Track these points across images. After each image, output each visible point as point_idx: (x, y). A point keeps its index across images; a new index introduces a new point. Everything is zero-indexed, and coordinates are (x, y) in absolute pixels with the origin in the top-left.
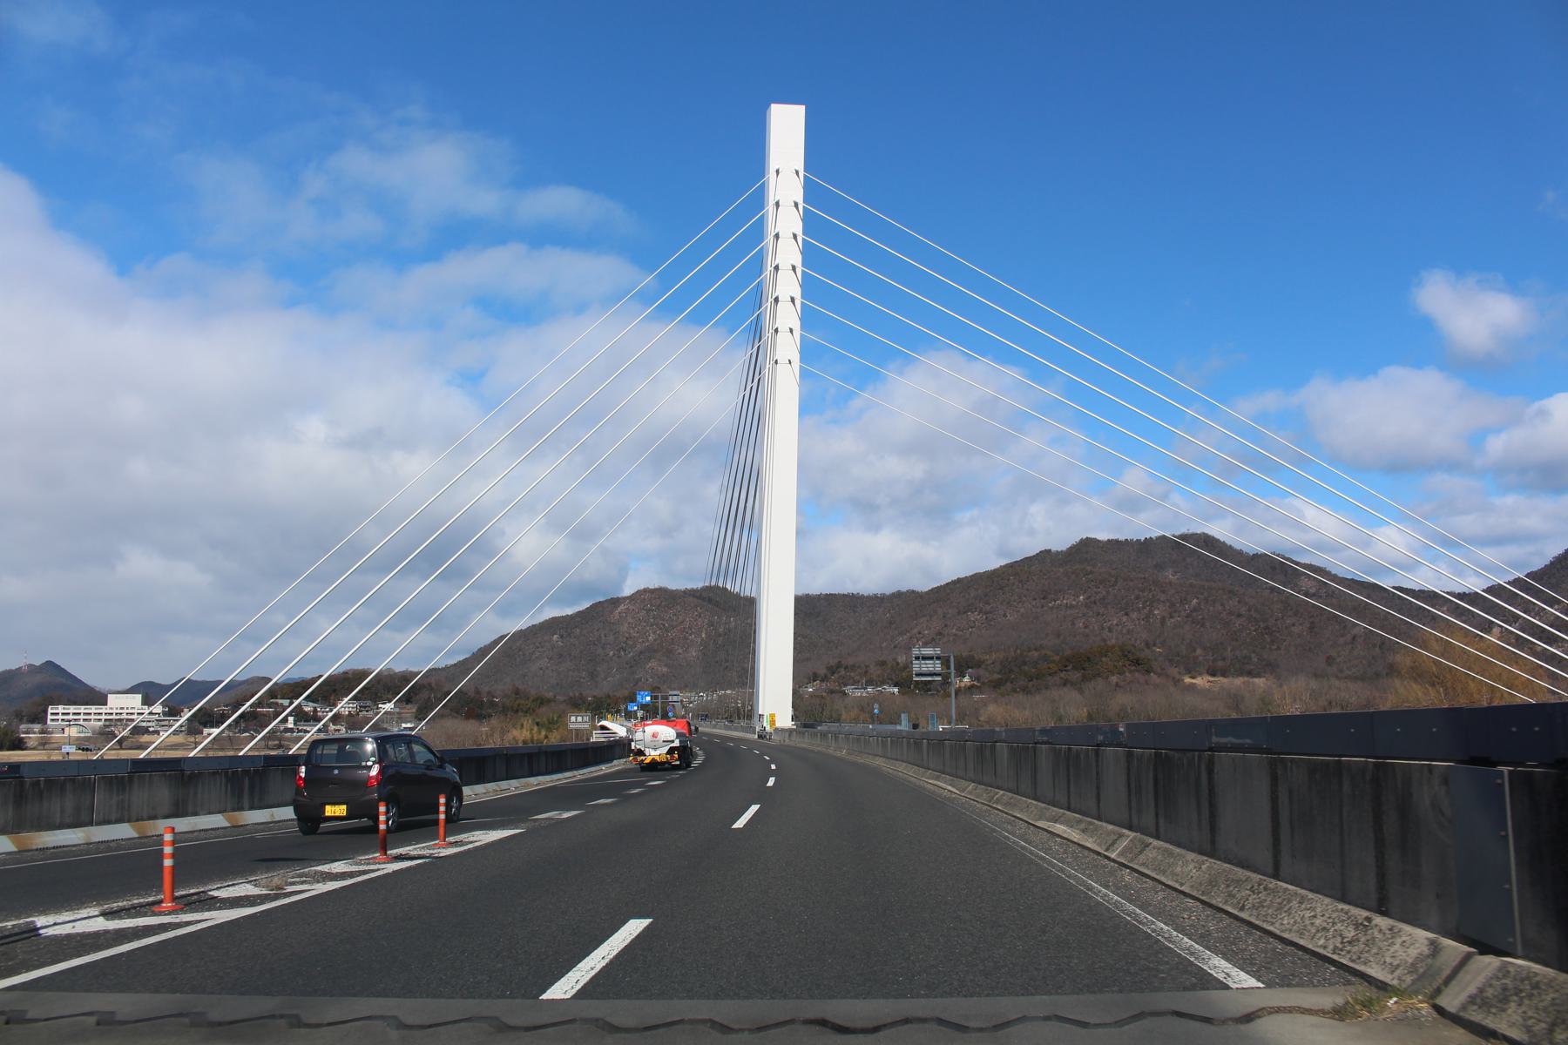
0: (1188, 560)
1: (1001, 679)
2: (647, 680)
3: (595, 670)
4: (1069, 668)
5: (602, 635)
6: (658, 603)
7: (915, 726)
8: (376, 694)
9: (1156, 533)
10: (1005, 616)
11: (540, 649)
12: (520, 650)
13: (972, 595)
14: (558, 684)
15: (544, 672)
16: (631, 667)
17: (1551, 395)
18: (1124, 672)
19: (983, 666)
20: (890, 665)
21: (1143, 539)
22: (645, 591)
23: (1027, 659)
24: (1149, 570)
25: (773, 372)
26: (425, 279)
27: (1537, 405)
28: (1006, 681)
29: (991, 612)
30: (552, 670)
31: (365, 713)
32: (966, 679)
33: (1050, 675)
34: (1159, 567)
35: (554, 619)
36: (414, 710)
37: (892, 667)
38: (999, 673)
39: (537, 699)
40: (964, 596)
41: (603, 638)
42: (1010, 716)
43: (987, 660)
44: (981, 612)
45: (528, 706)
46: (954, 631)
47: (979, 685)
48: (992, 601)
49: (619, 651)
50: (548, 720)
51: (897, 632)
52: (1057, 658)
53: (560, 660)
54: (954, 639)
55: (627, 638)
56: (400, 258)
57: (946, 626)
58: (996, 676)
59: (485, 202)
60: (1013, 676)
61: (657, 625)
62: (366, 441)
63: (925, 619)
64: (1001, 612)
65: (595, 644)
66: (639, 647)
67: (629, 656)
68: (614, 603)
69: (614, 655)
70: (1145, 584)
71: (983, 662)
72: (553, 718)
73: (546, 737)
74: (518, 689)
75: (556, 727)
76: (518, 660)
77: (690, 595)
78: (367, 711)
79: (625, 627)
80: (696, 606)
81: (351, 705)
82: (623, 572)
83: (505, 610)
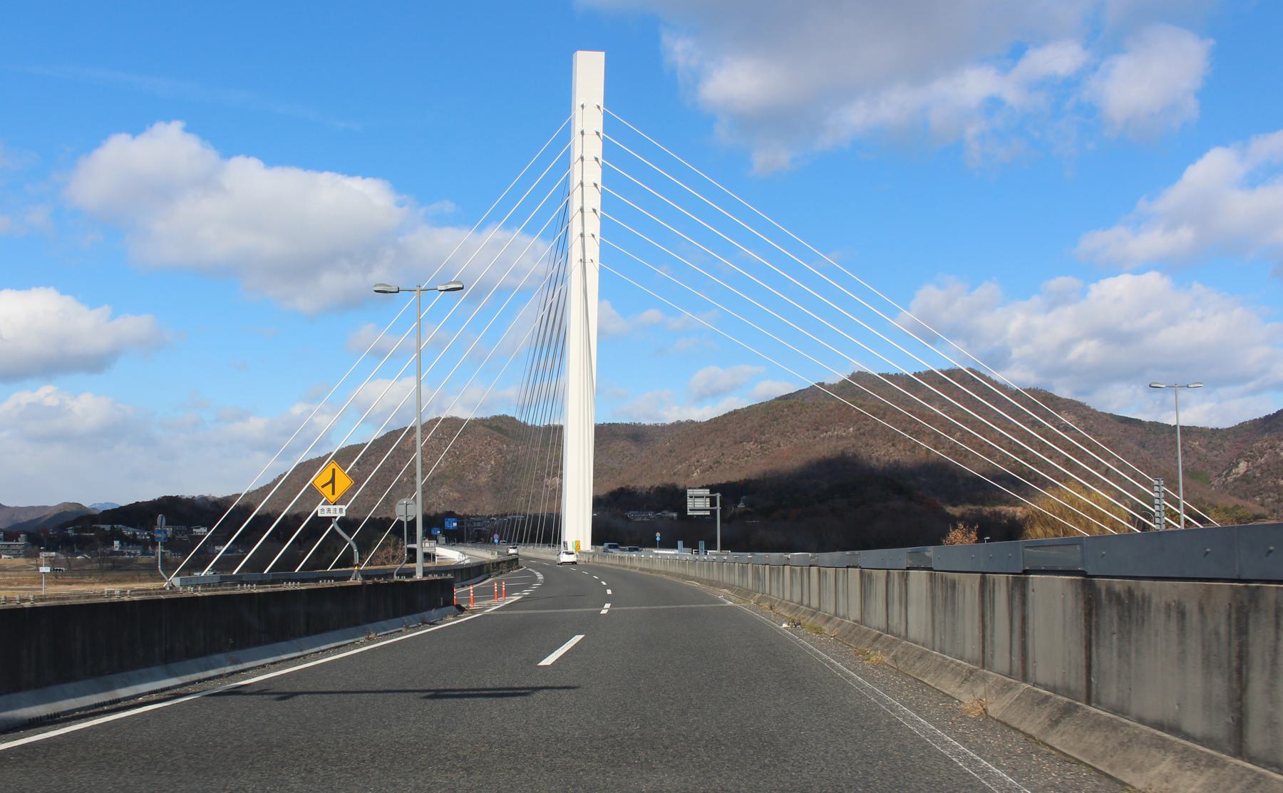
41: (397, 465)
44: (756, 441)
57: (723, 454)
63: (703, 448)
69: (408, 481)
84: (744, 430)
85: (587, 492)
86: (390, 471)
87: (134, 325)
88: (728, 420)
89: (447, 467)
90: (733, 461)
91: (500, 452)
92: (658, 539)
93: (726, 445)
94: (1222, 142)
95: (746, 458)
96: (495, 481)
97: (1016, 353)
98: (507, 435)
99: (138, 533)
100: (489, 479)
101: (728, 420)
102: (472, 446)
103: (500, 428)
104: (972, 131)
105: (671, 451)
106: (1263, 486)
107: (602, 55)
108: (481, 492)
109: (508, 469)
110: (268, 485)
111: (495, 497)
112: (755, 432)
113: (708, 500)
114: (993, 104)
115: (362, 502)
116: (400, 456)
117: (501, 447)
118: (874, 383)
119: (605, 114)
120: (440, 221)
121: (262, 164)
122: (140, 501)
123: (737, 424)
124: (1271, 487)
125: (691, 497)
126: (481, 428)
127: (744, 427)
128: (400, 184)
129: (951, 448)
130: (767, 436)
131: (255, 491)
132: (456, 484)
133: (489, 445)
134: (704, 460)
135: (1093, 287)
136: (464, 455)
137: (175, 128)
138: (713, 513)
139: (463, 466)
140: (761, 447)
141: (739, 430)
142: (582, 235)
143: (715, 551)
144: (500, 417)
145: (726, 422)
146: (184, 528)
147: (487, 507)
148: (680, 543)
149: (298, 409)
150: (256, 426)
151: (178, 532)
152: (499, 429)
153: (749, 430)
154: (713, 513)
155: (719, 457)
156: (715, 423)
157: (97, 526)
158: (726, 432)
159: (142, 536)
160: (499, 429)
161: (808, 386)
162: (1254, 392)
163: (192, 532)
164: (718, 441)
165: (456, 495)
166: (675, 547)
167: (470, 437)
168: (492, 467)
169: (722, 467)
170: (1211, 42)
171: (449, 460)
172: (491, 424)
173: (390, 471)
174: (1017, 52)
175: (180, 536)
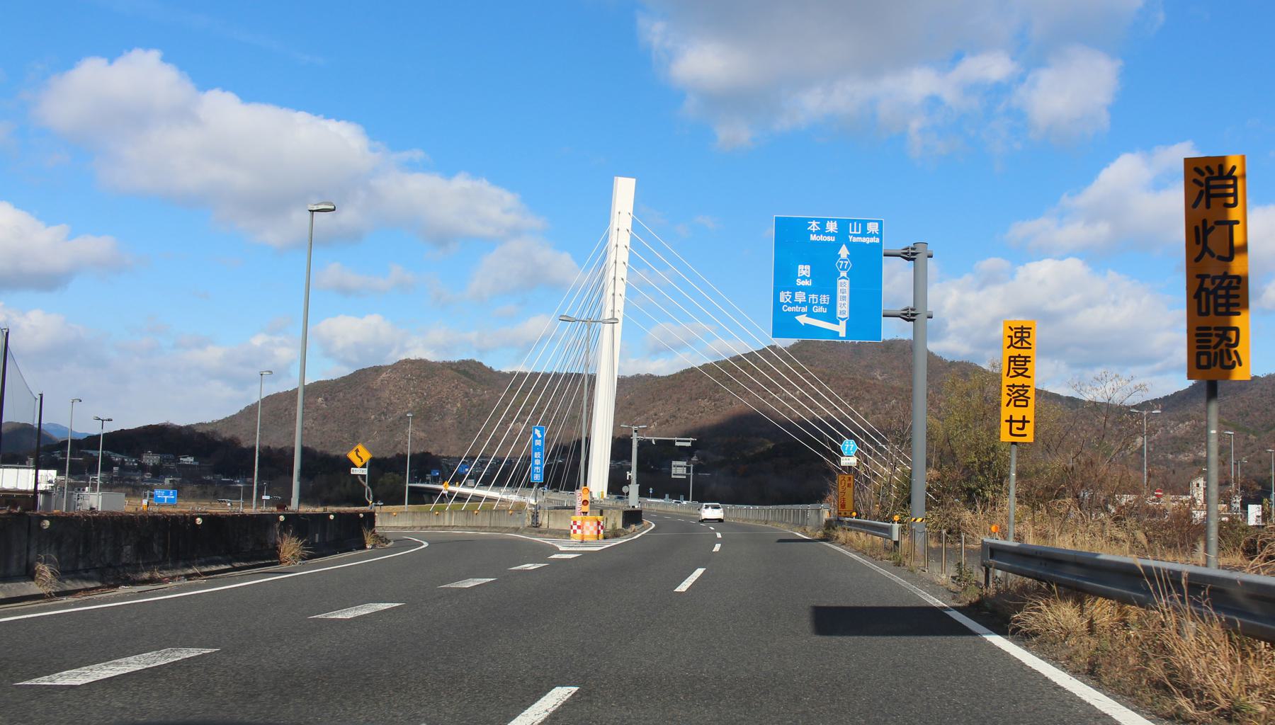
3: (357, 432)
12: (286, 410)
41: (366, 402)
44: (710, 399)
47: (704, 464)
57: (679, 409)
63: (660, 402)
69: (376, 418)
79: (386, 394)
80: (453, 378)
84: (700, 387)
85: (606, 465)
86: (357, 408)
87: (94, 245)
88: (685, 377)
89: (414, 407)
90: (688, 416)
91: (466, 395)
92: (651, 492)
93: (682, 401)
94: (1130, 149)
95: (700, 414)
96: (460, 423)
97: (952, 325)
98: (473, 379)
99: (126, 460)
100: (454, 421)
101: (685, 377)
102: (439, 388)
103: (468, 372)
104: (915, 125)
105: (630, 404)
106: (1154, 459)
107: (634, 180)
108: (446, 433)
109: (474, 412)
110: (234, 416)
111: (460, 438)
112: (710, 390)
113: (685, 469)
114: (934, 102)
115: (329, 437)
116: (368, 394)
117: (467, 390)
118: (822, 349)
119: (633, 218)
120: (412, 167)
121: (238, 100)
122: (125, 429)
123: (694, 381)
124: (1161, 461)
125: (674, 466)
126: (449, 371)
127: (699, 384)
128: (374, 130)
129: (886, 414)
130: (720, 394)
131: (219, 421)
132: (423, 424)
133: (457, 388)
134: (662, 414)
135: (1020, 269)
136: (431, 397)
137: (154, 56)
138: (688, 477)
139: (430, 407)
140: (715, 404)
141: (694, 387)
142: (614, 295)
143: (663, 501)
144: (467, 361)
145: (683, 379)
146: (171, 456)
147: (451, 447)
148: (667, 496)
149: (258, 341)
150: (213, 355)
151: (165, 460)
152: (466, 373)
153: (704, 388)
154: (688, 477)
155: (676, 412)
156: (673, 379)
157: (85, 451)
158: (683, 388)
159: (130, 463)
160: (466, 373)
161: (761, 348)
162: (1161, 372)
163: (179, 461)
164: (675, 397)
165: (423, 435)
166: (663, 497)
167: (438, 380)
168: (458, 409)
169: (677, 422)
170: (1120, 63)
171: (417, 400)
172: (458, 368)
173: (357, 408)
174: (958, 58)
175: (167, 464)
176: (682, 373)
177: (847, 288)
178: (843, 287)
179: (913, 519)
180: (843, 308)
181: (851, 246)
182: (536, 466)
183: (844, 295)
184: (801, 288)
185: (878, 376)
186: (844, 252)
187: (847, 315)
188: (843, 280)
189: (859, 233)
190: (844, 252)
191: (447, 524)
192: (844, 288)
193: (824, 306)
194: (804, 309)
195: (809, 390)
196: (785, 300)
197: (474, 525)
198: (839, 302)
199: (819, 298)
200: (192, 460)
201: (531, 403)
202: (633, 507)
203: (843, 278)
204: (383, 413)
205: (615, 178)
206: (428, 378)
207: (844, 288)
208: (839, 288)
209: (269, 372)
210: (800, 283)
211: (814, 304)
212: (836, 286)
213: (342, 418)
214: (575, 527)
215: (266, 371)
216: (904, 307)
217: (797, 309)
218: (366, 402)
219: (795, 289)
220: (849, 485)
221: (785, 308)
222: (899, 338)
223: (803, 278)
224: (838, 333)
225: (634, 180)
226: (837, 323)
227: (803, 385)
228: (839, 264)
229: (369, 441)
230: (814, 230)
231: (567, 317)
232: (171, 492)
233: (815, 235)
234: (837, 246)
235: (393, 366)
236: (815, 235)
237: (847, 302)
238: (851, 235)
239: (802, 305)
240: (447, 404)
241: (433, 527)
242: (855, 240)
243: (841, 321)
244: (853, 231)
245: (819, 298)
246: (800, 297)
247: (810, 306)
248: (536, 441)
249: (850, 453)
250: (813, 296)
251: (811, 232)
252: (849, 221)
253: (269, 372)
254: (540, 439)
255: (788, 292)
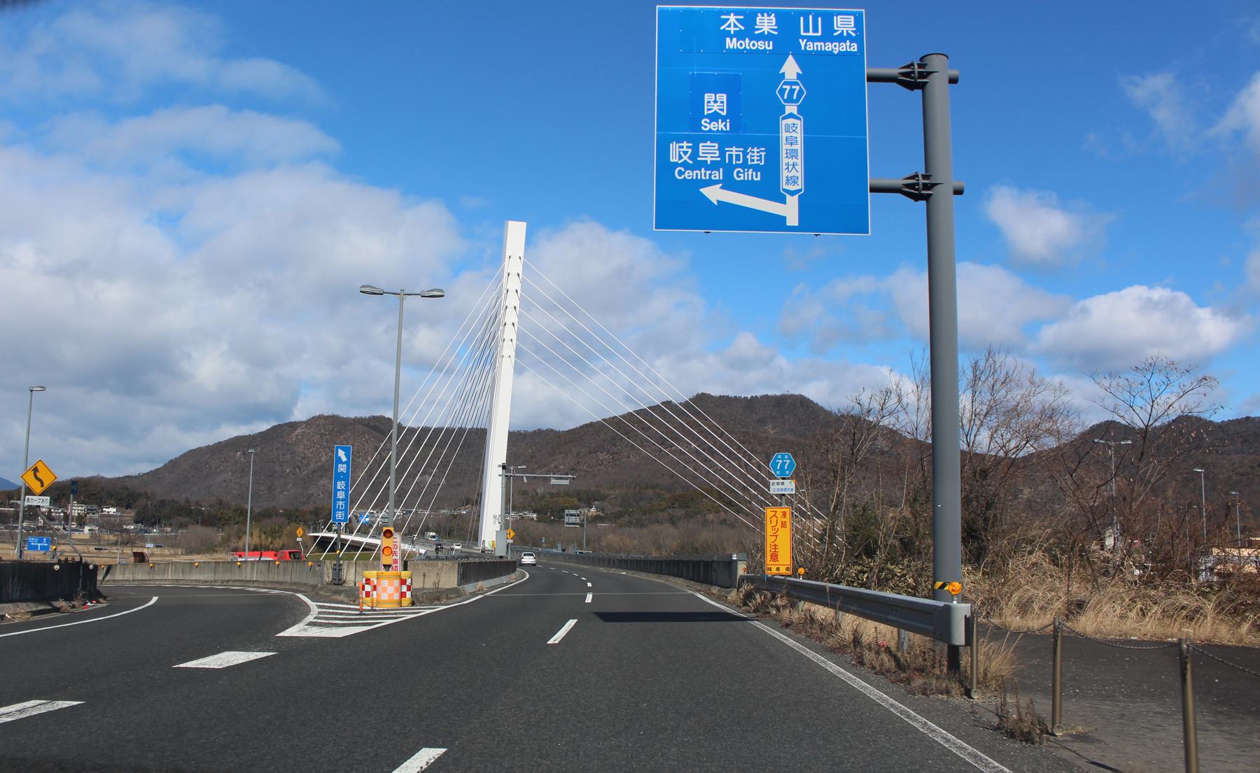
0: (786, 416)
1: (620, 512)
2: (319, 495)
3: (273, 484)
4: (676, 506)
5: (281, 454)
6: (331, 429)
7: (564, 550)
8: (101, 499)
9: (760, 392)
10: (628, 457)
11: (225, 464)
12: (207, 463)
13: (602, 438)
14: (239, 495)
15: (227, 484)
16: (305, 483)
17: (1092, 296)
18: (720, 512)
19: (607, 500)
20: (530, 494)
21: (749, 397)
22: (321, 417)
23: (643, 496)
24: (752, 424)
25: (501, 363)
26: (133, 130)
27: (1081, 303)
28: (625, 514)
29: (617, 453)
30: (235, 483)
31: (91, 515)
32: (593, 510)
33: (661, 510)
34: (762, 422)
35: (237, 438)
36: (133, 515)
37: (532, 497)
38: (620, 506)
39: (237, 510)
40: (594, 438)
41: (281, 456)
42: (623, 543)
43: (611, 495)
44: (608, 452)
45: (230, 515)
46: (585, 467)
47: (603, 515)
48: (618, 444)
49: (294, 468)
50: (271, 530)
51: (537, 466)
52: (668, 496)
53: (243, 474)
54: (585, 474)
55: (302, 458)
56: (113, 112)
57: (578, 462)
58: (618, 509)
59: (195, 68)
60: (631, 510)
61: (328, 447)
62: (69, 271)
63: (561, 456)
64: (626, 454)
65: (274, 462)
66: (312, 466)
67: (303, 473)
68: (292, 427)
69: (291, 472)
70: (746, 438)
71: (608, 496)
72: (275, 529)
73: (271, 543)
74: (221, 500)
75: (278, 535)
76: (205, 472)
77: (359, 423)
78: (93, 514)
79: (301, 448)
80: (364, 433)
81: (80, 508)
82: (294, 398)
83: (187, 425)
99: (53, 510)
107: (524, 224)
133: (367, 442)
176: (581, 427)
177: (799, 135)
178: (792, 133)
179: (939, 584)
180: (793, 171)
181: (804, 59)
182: (339, 500)
183: (794, 147)
184: (711, 137)
185: (770, 430)
186: (791, 69)
187: (800, 185)
188: (791, 121)
189: (819, 34)
190: (791, 69)
191: (248, 579)
192: (794, 134)
193: (756, 168)
194: (718, 175)
195: (701, 444)
196: (680, 158)
197: (276, 580)
198: (784, 160)
199: (745, 154)
200: (115, 510)
201: (435, 457)
202: (501, 557)
203: (791, 116)
204: (298, 466)
205: (506, 222)
206: (341, 433)
207: (794, 134)
208: (784, 135)
209: (42, 387)
210: (707, 125)
211: (738, 166)
212: (777, 130)
213: (259, 471)
214: (368, 588)
215: (37, 387)
216: (912, 173)
217: (702, 174)
218: (281, 456)
219: (697, 138)
220: (783, 525)
221: (681, 173)
222: (790, 393)
223: (714, 117)
224: (784, 218)
225: (524, 224)
226: (782, 200)
227: (696, 440)
228: (782, 91)
229: (285, 493)
230: (732, 29)
231: (371, 287)
232: (45, 539)
233: (734, 40)
234: (778, 58)
235: (307, 421)
236: (734, 40)
237: (799, 161)
238: (803, 38)
239: (714, 166)
240: (358, 457)
241: (234, 581)
242: (811, 47)
243: (788, 196)
244: (806, 30)
245: (745, 154)
246: (709, 152)
247: (729, 169)
248: (340, 465)
249: (785, 474)
250: (734, 151)
251: (727, 34)
252: (799, 14)
253: (42, 387)
254: (344, 463)
255: (685, 144)
